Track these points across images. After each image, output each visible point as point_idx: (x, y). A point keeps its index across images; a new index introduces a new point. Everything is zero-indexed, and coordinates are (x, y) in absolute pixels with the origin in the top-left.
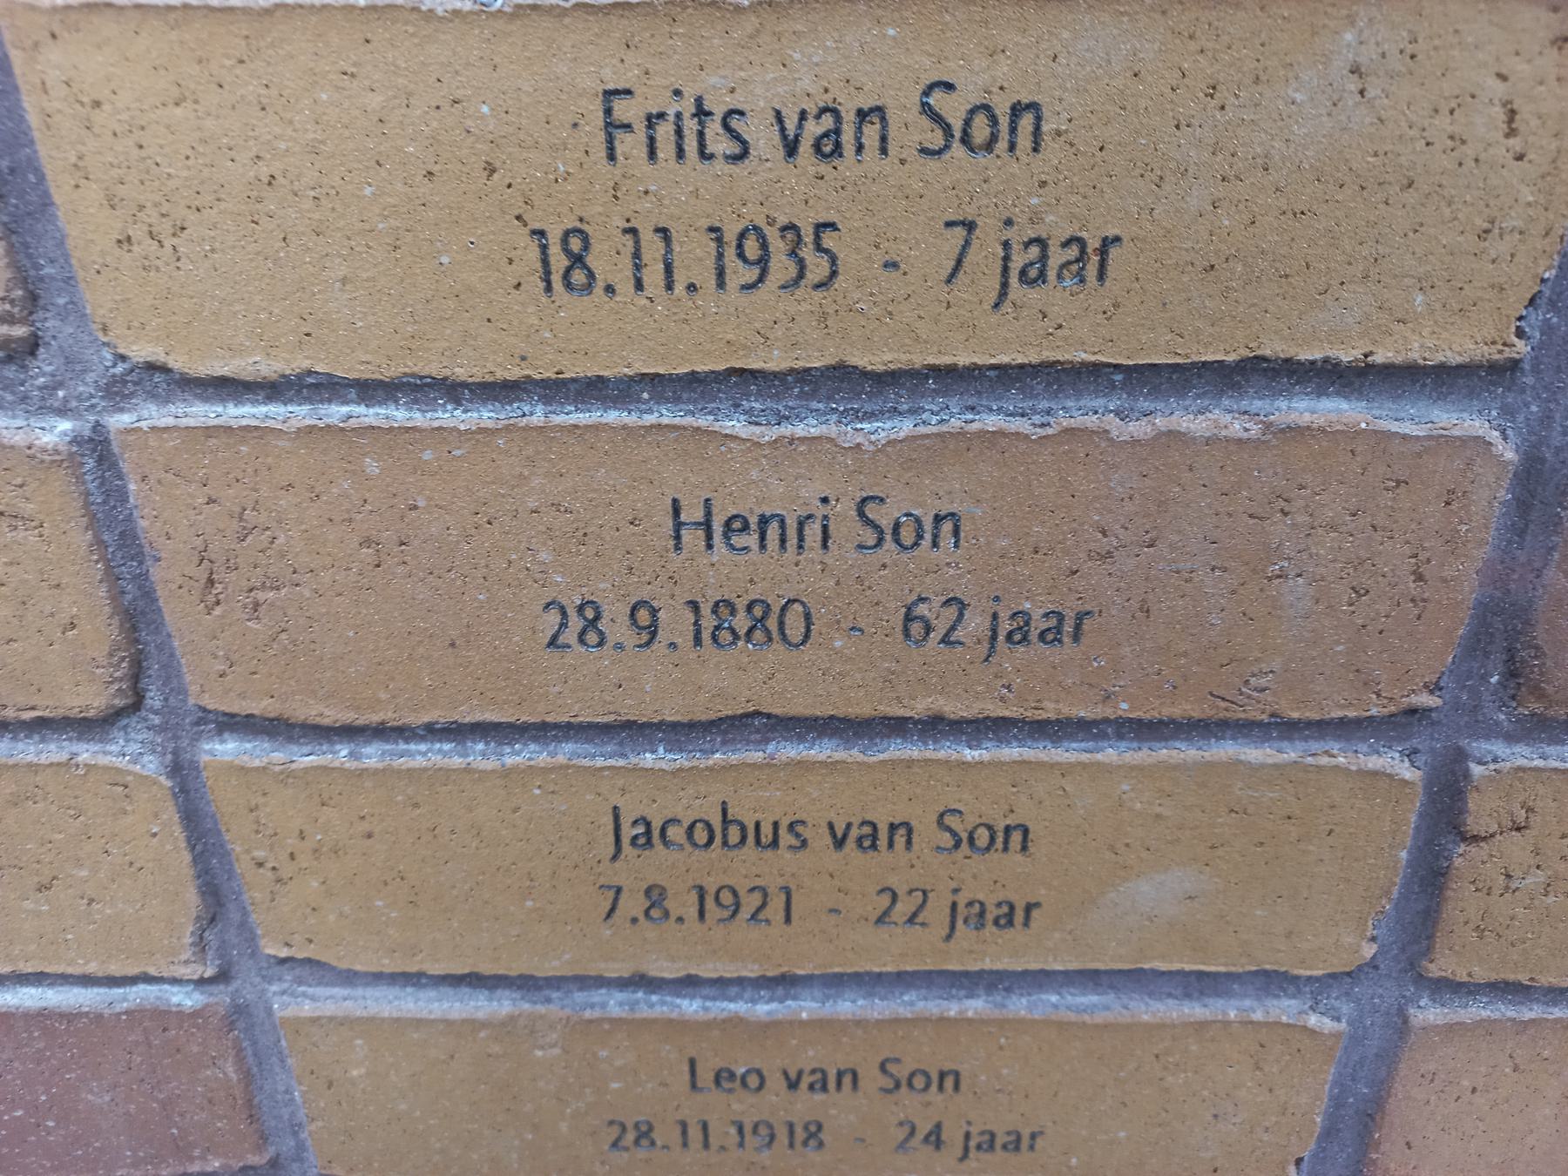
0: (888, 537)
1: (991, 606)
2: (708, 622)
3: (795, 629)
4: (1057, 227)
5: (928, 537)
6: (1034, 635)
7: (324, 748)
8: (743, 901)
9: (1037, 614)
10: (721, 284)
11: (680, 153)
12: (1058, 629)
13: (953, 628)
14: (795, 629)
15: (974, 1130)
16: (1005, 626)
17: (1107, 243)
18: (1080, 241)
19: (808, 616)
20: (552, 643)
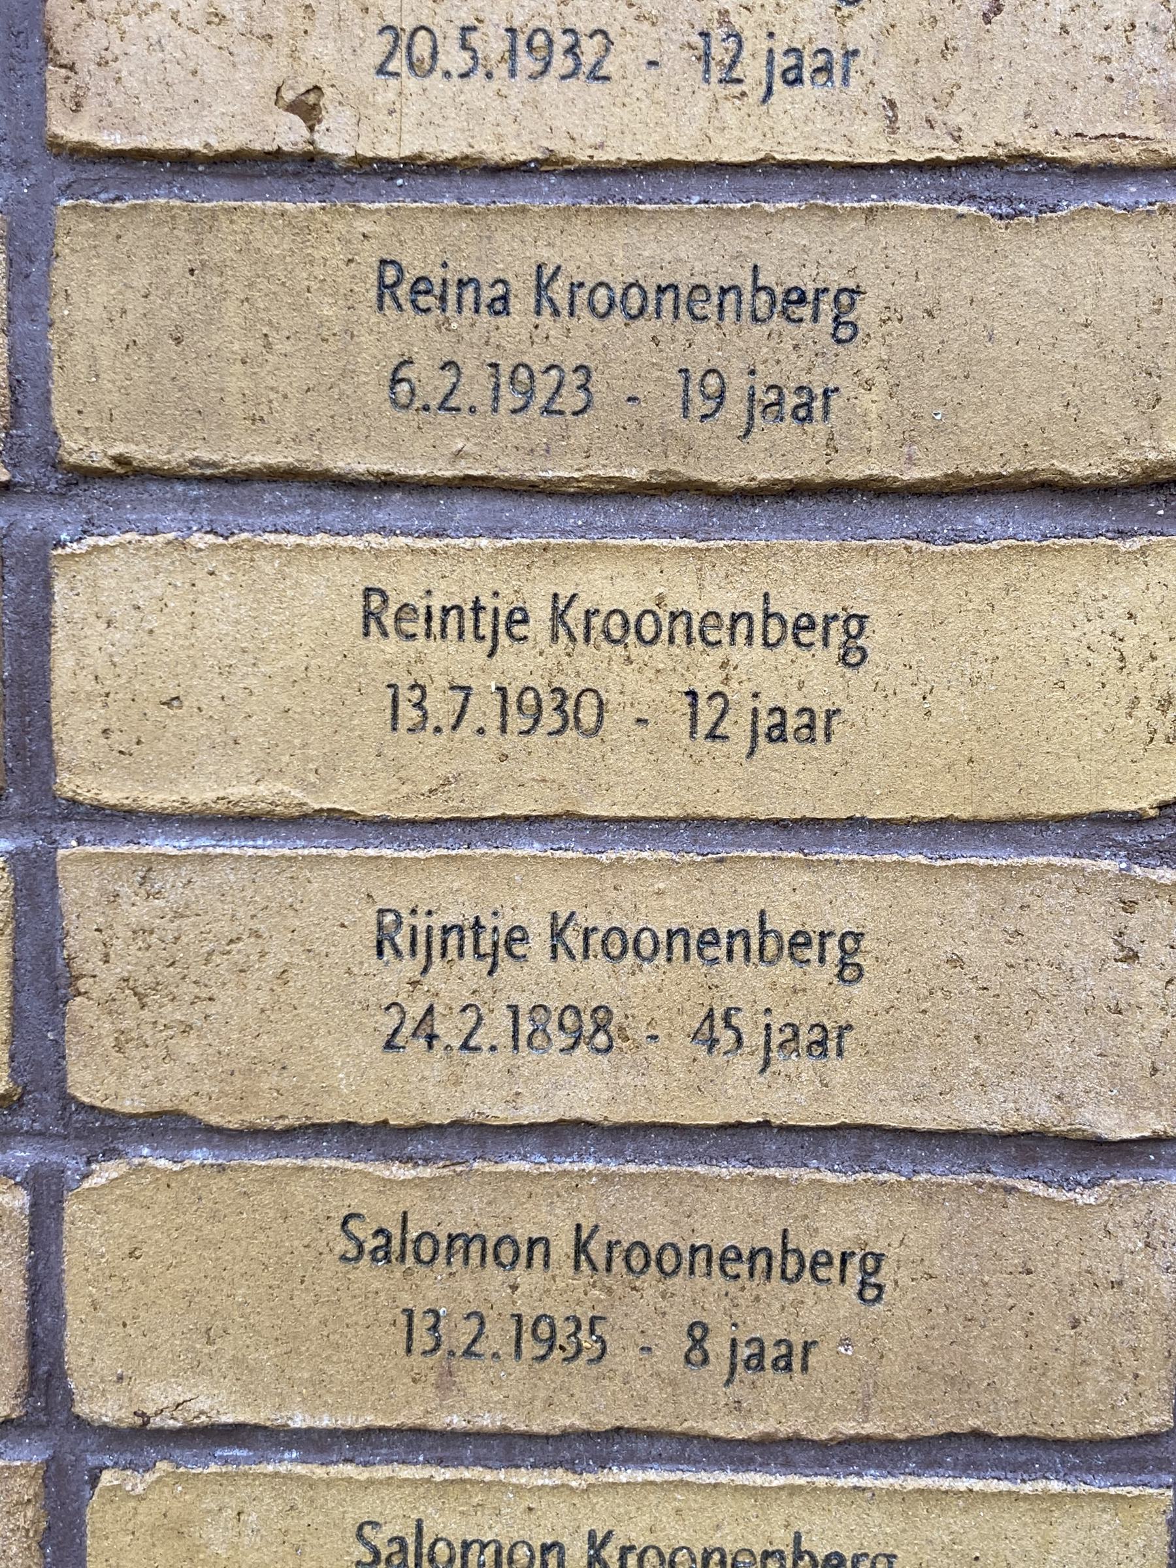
0: (653, 1264)
1: (766, 44)
2: (526, 1027)
3: (588, 717)
4: (771, 1332)
5: (686, 1265)
6: (768, 1363)
7: (260, 1146)
8: (567, 379)
9: (791, 710)
10: (503, 729)
11: (461, 635)
12: (810, 727)
13: (716, 725)
14: (588, 717)
15: (743, 1338)
16: (744, 1352)
17: (830, 715)
18: (811, 711)
19: (601, 704)
20: (381, 70)
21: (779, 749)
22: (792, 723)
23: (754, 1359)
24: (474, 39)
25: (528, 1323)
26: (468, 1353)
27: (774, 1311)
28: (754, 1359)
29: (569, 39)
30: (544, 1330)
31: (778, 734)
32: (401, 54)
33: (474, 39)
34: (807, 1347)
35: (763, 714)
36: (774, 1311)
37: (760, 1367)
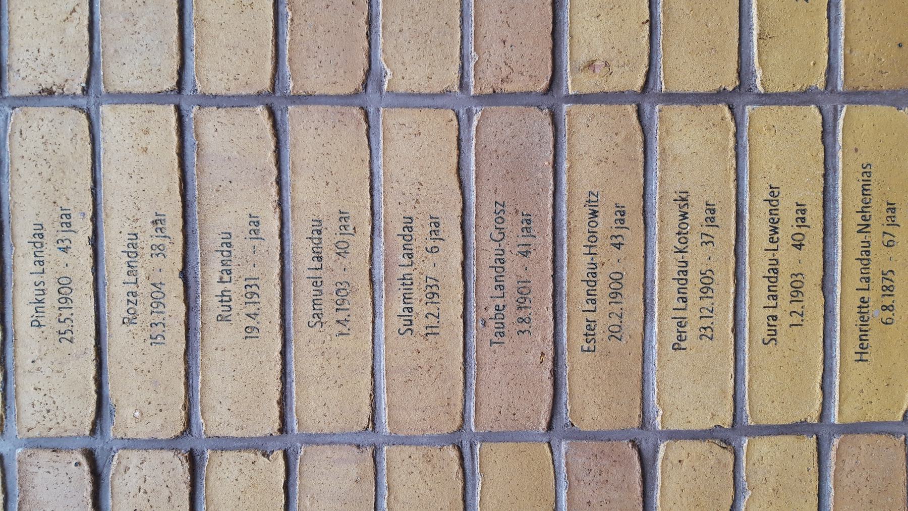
2: (888, 292)
6: (68, 221)
17: (888, 204)
21: (808, 219)
22: (801, 216)
23: (711, 220)
24: (62, 331)
25: (612, 300)
26: (802, 315)
27: (788, 215)
28: (711, 220)
29: (429, 288)
30: (705, 290)
31: (69, 224)
32: (616, 335)
33: (62, 331)
34: (888, 204)
35: (63, 229)
36: (788, 215)
37: (713, 218)
